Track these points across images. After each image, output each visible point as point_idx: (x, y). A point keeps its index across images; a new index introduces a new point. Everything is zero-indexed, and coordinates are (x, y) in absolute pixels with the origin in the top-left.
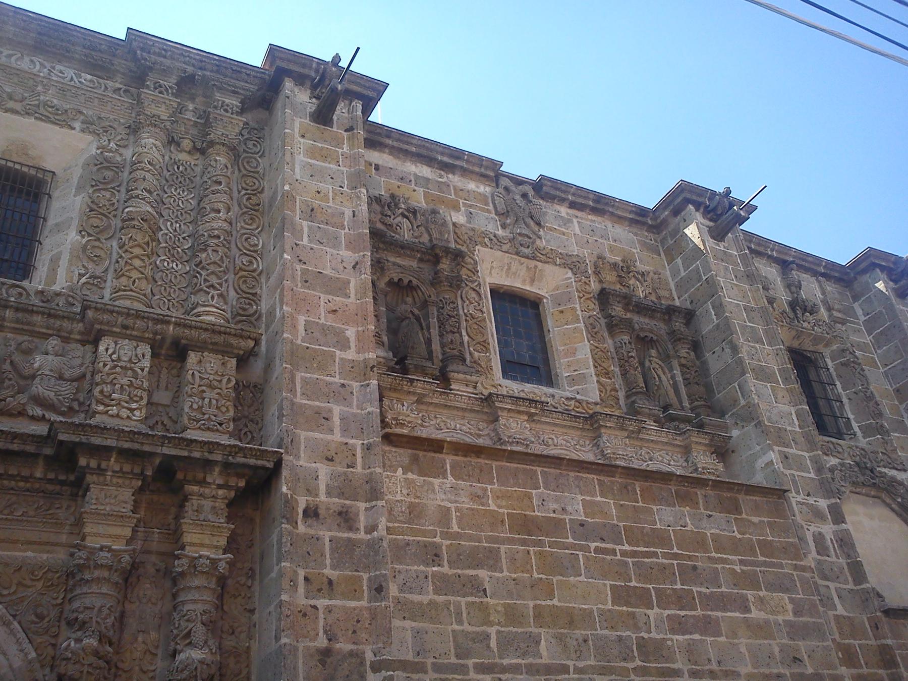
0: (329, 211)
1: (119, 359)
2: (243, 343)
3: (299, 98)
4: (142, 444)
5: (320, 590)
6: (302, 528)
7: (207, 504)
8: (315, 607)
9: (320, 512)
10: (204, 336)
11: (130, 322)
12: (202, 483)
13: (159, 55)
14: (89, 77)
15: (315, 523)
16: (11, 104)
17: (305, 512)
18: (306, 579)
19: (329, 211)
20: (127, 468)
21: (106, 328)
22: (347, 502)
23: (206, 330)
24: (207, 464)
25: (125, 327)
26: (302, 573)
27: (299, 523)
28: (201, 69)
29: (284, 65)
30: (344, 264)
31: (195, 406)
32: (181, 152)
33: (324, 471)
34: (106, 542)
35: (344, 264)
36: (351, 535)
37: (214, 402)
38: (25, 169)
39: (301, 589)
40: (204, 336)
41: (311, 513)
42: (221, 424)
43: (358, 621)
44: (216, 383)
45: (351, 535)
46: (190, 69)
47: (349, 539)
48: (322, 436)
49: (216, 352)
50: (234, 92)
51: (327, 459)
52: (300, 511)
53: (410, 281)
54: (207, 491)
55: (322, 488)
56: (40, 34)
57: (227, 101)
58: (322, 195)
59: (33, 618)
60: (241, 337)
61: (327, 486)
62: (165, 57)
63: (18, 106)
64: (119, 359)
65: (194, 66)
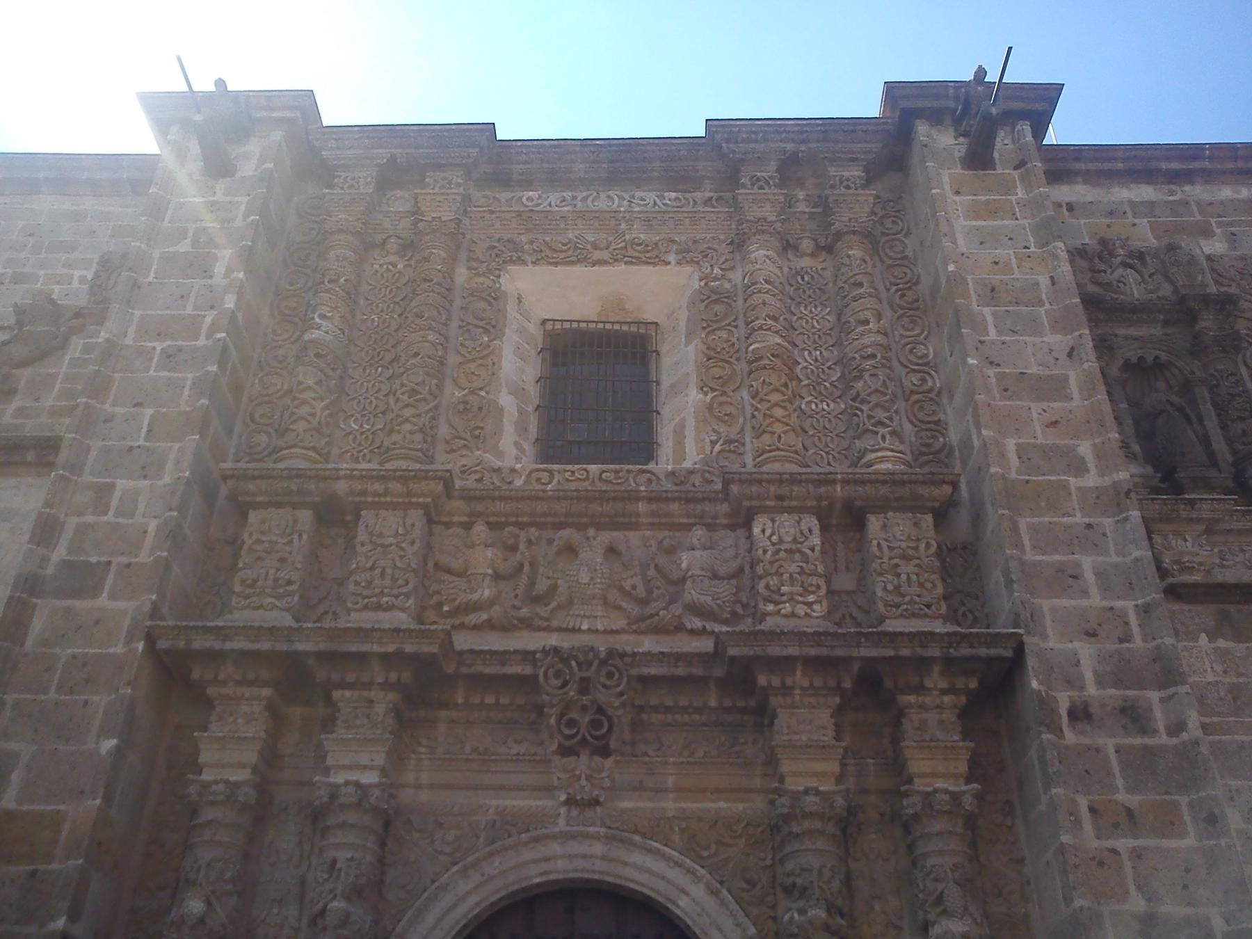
0: (1017, 285)
1: (781, 541)
2: (937, 492)
3: (941, 142)
4: (833, 647)
5: (1116, 825)
6: (1070, 737)
7: (932, 717)
8: (1114, 851)
9: (1092, 710)
10: (884, 490)
11: (785, 490)
12: (920, 689)
13: (749, 141)
14: (674, 195)
15: (1089, 729)
16: (597, 255)
17: (1072, 714)
18: (1092, 810)
19: (1017, 285)
20: (818, 682)
21: (755, 503)
22: (1130, 693)
23: (884, 482)
24: (922, 664)
25: (780, 498)
26: (1083, 803)
27: (1065, 729)
28: (803, 142)
29: (910, 104)
30: (1055, 354)
31: (890, 587)
32: (801, 256)
33: (1086, 652)
34: (812, 783)
35: (1055, 354)
36: (1148, 741)
37: (914, 577)
38: (625, 328)
39: (1088, 826)
40: (884, 490)
41: (1080, 714)
42: (928, 606)
43: (1188, 870)
44: (911, 552)
45: (1148, 741)
46: (790, 147)
47: (1145, 747)
48: (1073, 602)
49: (903, 509)
50: (853, 160)
51: (1088, 634)
52: (1064, 713)
53: (1157, 358)
54: (928, 700)
55: (1089, 676)
56: (612, 162)
57: (846, 174)
58: (1001, 265)
59: (743, 885)
60: (933, 483)
61: (1095, 673)
62: (756, 141)
63: (605, 255)
64: (781, 541)
65: (793, 140)
